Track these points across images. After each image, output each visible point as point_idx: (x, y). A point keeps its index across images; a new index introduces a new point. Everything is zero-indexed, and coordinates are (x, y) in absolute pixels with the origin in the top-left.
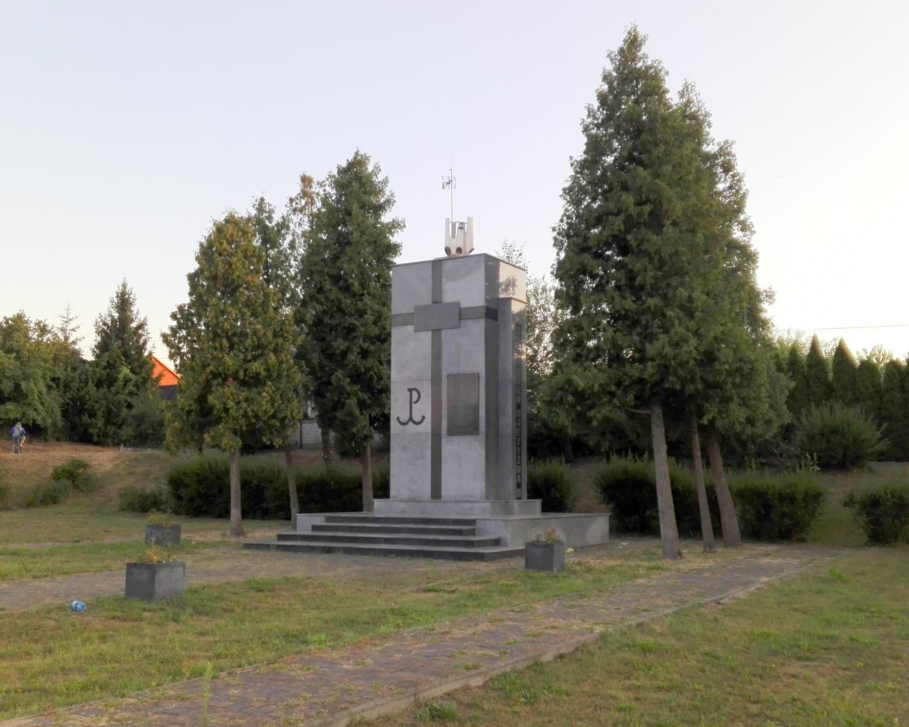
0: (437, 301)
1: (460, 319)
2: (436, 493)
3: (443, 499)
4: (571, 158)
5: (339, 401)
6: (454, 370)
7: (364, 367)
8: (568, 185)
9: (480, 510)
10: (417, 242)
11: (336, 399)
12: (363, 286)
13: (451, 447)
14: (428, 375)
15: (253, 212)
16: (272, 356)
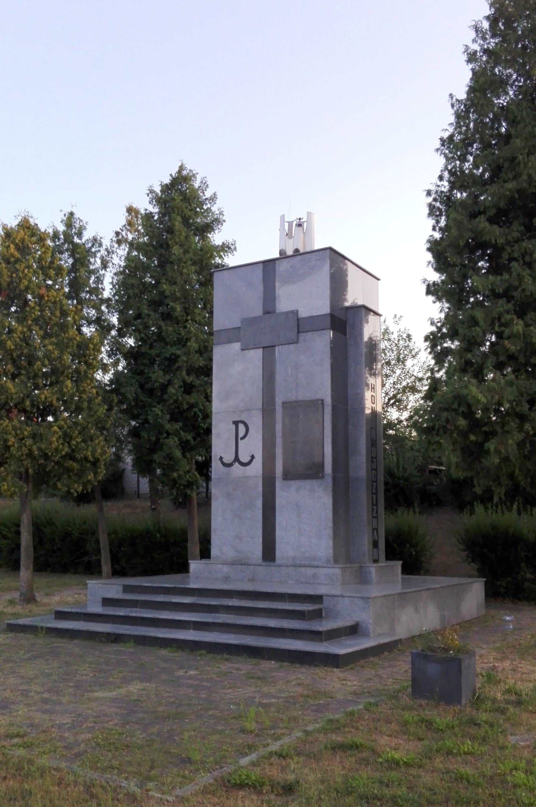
0: (269, 309)
1: (299, 332)
2: (269, 552)
3: (278, 561)
4: (451, 96)
5: (158, 440)
7: (188, 403)
8: (446, 135)
9: (328, 581)
10: (246, 236)
11: (154, 439)
12: (187, 311)
13: (287, 495)
15: (61, 228)
16: (69, 383)
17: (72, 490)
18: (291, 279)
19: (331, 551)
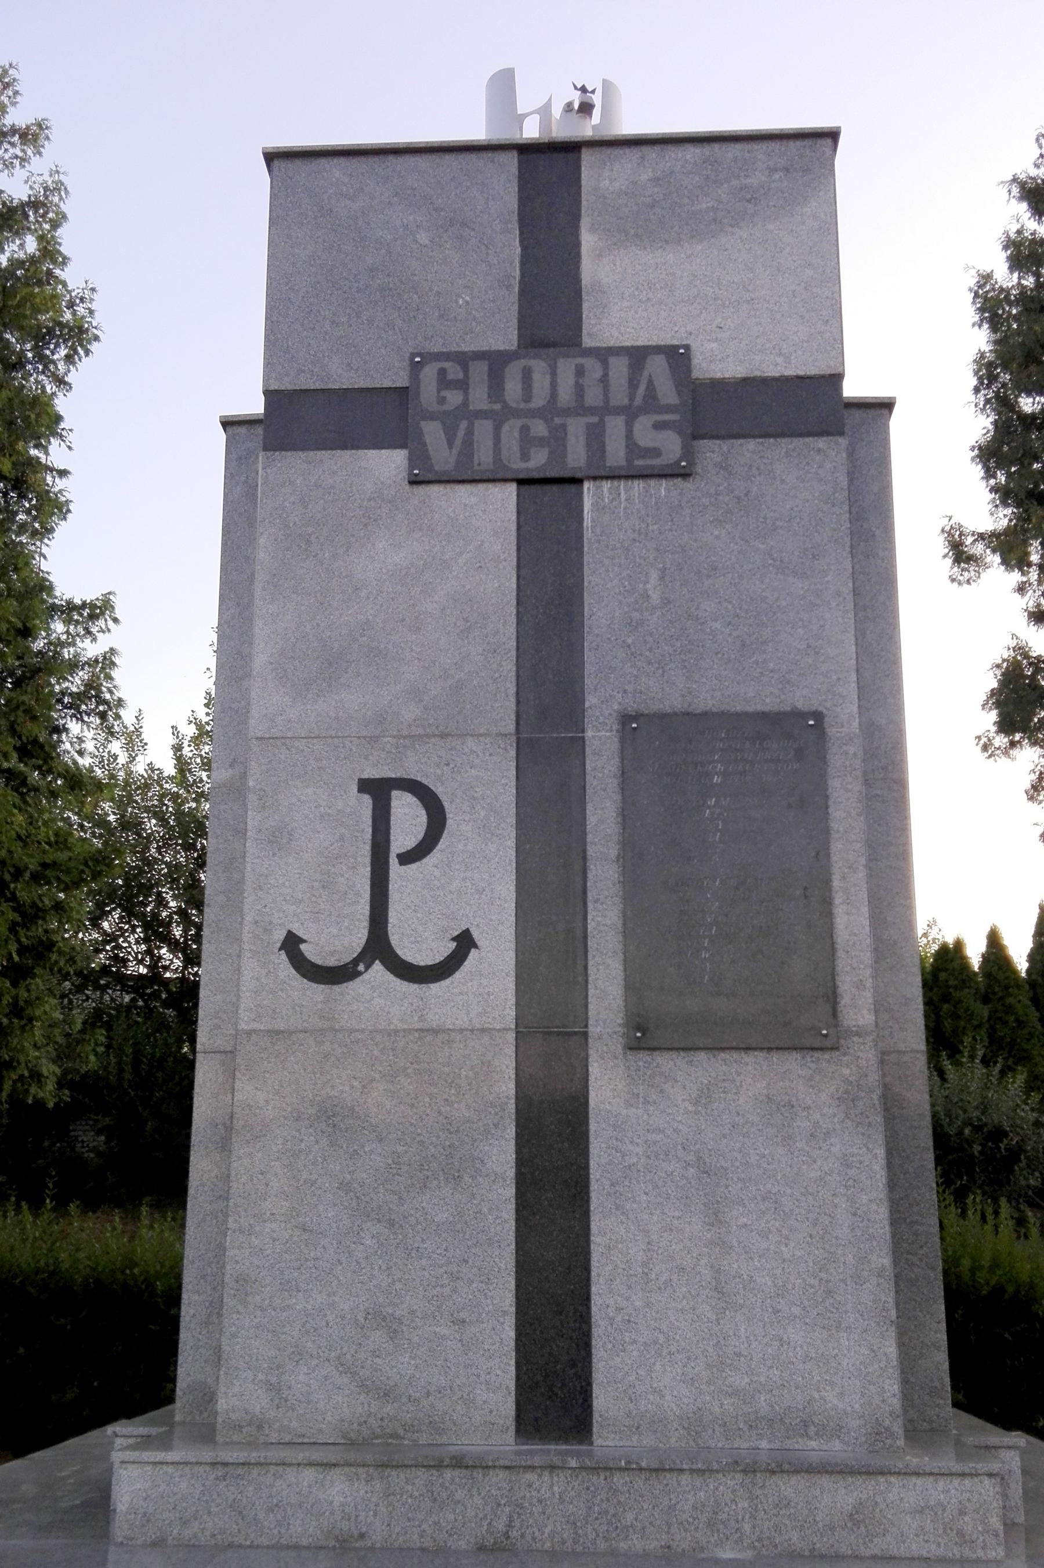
2: (555, 1391)
3: (605, 1439)
6: (669, 693)
14: (501, 709)
17: (1018, 1122)
18: (647, 224)
19: (893, 1387)
